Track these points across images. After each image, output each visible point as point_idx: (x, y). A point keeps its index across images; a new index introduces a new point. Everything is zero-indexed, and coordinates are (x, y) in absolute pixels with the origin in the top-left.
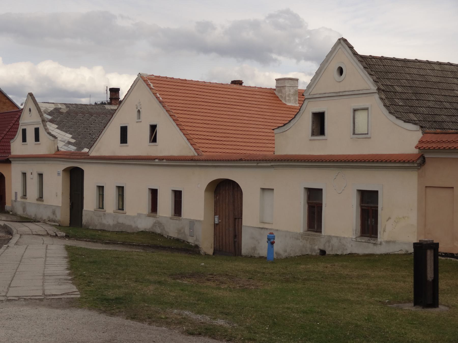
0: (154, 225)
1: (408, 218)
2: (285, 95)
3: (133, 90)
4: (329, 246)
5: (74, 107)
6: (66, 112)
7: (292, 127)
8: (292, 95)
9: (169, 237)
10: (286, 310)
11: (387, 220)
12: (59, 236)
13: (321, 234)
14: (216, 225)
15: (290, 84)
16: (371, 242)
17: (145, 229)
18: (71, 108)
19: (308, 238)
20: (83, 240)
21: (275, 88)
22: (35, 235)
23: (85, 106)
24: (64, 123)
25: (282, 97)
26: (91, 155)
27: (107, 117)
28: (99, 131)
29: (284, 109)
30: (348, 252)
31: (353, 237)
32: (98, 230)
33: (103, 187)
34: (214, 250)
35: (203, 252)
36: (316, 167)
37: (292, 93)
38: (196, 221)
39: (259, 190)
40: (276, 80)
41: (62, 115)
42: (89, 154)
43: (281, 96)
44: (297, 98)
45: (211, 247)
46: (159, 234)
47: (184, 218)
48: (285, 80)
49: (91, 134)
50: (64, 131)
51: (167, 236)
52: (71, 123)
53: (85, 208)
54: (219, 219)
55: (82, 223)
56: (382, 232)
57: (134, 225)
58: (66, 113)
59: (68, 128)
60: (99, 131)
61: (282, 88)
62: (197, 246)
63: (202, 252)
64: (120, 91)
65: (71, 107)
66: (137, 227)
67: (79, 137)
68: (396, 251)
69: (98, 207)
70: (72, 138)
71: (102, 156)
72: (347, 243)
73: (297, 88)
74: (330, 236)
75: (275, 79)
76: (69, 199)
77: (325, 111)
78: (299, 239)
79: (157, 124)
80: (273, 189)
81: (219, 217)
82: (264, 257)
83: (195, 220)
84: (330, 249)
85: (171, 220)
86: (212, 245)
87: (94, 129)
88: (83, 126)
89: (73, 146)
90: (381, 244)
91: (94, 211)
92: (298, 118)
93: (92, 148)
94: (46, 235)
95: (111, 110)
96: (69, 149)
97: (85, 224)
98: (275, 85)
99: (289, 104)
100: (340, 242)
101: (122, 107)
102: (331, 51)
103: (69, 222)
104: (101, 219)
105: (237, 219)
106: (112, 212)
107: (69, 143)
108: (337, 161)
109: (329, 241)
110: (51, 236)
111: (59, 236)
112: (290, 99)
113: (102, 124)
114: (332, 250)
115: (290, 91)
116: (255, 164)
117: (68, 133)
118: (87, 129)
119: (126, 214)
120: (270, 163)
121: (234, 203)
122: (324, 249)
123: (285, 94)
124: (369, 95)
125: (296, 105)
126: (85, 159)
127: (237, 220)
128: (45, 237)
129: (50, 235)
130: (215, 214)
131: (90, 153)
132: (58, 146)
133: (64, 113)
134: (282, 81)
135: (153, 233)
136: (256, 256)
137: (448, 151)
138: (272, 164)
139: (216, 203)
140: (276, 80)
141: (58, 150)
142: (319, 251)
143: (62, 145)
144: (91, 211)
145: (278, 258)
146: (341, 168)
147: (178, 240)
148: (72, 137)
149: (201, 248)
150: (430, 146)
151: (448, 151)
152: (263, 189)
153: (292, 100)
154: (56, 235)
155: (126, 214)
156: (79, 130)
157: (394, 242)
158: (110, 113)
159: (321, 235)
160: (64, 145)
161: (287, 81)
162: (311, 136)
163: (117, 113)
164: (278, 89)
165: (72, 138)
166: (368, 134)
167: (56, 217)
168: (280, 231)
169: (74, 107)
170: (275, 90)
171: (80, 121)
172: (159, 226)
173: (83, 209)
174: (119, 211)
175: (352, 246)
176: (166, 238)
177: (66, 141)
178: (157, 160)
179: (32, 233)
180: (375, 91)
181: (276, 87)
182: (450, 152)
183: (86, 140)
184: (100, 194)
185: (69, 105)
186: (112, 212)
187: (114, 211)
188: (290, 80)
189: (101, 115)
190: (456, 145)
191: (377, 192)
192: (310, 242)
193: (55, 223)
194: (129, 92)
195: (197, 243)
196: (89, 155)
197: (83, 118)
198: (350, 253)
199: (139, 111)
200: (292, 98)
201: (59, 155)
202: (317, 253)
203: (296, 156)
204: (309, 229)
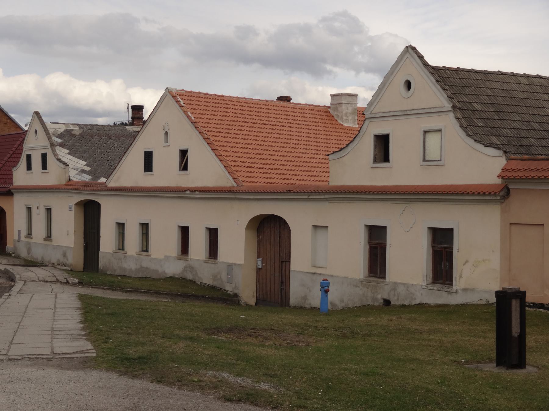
0: (185, 269)
1: (489, 261)
2: (341, 114)
3: (159, 108)
4: (394, 295)
5: (89, 128)
6: (79, 134)
7: (349, 152)
8: (351, 113)
9: (202, 284)
10: (343, 372)
11: (464, 264)
12: (70, 282)
13: (384, 281)
14: (258, 270)
15: (347, 101)
16: (445, 290)
17: (174, 274)
18: (86, 129)
19: (369, 285)
20: (100, 288)
21: (329, 105)
22: (42, 281)
23: (102, 127)
24: (77, 147)
25: (338, 116)
26: (109, 186)
27: (128, 140)
28: (119, 158)
29: (341, 131)
30: (418, 302)
31: (423, 284)
32: (118, 275)
33: (123, 224)
34: (257, 299)
35: (243, 301)
36: (379, 201)
37: (350, 112)
38: (235, 264)
39: (310, 228)
40: (331, 96)
41: (74, 137)
42: (107, 185)
43: (336, 115)
44: (356, 118)
45: (253, 297)
46: (191, 281)
47: (221, 261)
48: (341, 96)
49: (109, 161)
50: (76, 157)
51: (201, 282)
52: (85, 147)
53: (102, 249)
54: (263, 262)
55: (98, 268)
56: (458, 278)
57: (160, 270)
58: (79, 135)
59: (82, 154)
60: (119, 158)
61: (337, 105)
62: (236, 295)
63: (243, 302)
64: (143, 109)
65: (85, 128)
66: (164, 272)
67: (95, 164)
68: (475, 301)
69: (118, 248)
70: (86, 165)
71: (122, 187)
72: (416, 291)
73: (356, 105)
74: (395, 283)
75: (330, 95)
76: (83, 239)
77: (389, 133)
78: (359, 287)
79: (188, 149)
80: (327, 227)
81: (263, 259)
82: (316, 307)
83: (234, 264)
84: (396, 298)
85: (206, 264)
86: (254, 294)
87: (113, 155)
88: (99, 151)
89: (87, 174)
90: (456, 292)
91: (112, 252)
92: (357, 142)
93: (110, 177)
94: (55, 282)
95: (134, 132)
96: (83, 179)
97: (102, 268)
98: (330, 102)
99: (346, 125)
100: (408, 290)
101: (147, 128)
102: (396, 61)
103: (83, 265)
104: (122, 262)
105: (285, 263)
106: (134, 254)
107: (83, 171)
108: (404, 193)
109: (394, 289)
110: (61, 283)
111: (70, 282)
112: (348, 119)
113: (123, 148)
114: (398, 299)
115: (348, 109)
116: (306, 197)
117: (81, 160)
118: (104, 155)
119: (151, 257)
120: (324, 195)
121: (280, 243)
122: (388, 299)
123: (342, 112)
124: (442, 114)
125: (355, 126)
126: (101, 190)
127: (284, 264)
128: (54, 283)
129: (60, 281)
130: (258, 257)
131: (108, 183)
132: (70, 175)
133: (77, 135)
134: (338, 97)
135: (183, 279)
136: (307, 306)
137: (537, 181)
138: (326, 196)
139: (259, 243)
140: (331, 96)
141: (70, 180)
142: (382, 301)
143: (75, 174)
144: (109, 253)
145: (333, 309)
146: (408, 201)
147: (213, 288)
148: (86, 164)
149: (241, 297)
150: (515, 174)
151: (537, 181)
152: (315, 227)
153: (351, 120)
154: (68, 282)
155: (151, 257)
156: (95, 155)
157: (472, 290)
158: (131, 135)
159: (385, 282)
160: (77, 174)
161: (344, 97)
162: (373, 163)
163: (140, 135)
164: (333, 106)
165: (86, 165)
166: (441, 160)
167: (67, 259)
168: (335, 276)
169: (89, 128)
170: (329, 107)
171: (96, 145)
172: (190, 271)
173: (100, 250)
174: (143, 252)
175: (422, 294)
176: (199, 285)
177: (79, 168)
178: (188, 192)
179: (39, 279)
180: (450, 109)
181: (331, 104)
182: (539, 182)
183: (103, 167)
184: (120, 232)
185: (82, 126)
186: (134, 254)
187: (136, 252)
188: (348, 96)
189: (121, 138)
190: (546, 174)
191: (452, 230)
192: (371, 290)
193: (66, 267)
194: (154, 110)
195: (236, 291)
196: (106, 186)
197: (99, 141)
198: (419, 304)
199: (166, 133)
200: (350, 118)
201: (70, 185)
202: (380, 303)
203: (355, 187)
204: (371, 275)
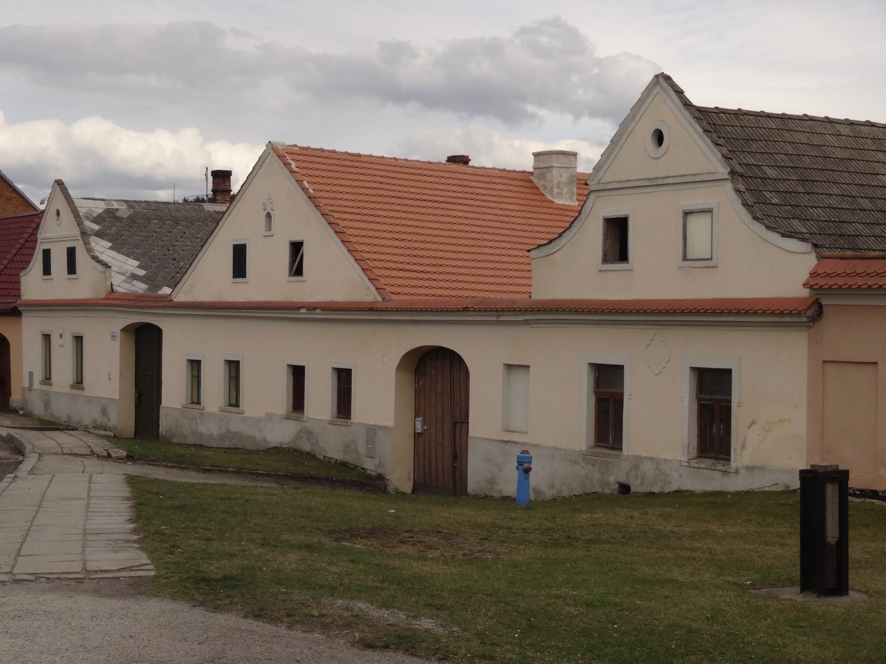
0: (299, 435)
1: (789, 422)
2: (551, 184)
3: (257, 175)
4: (636, 477)
5: (143, 206)
6: (128, 217)
7: (564, 245)
8: (566, 183)
9: (326, 459)
10: (553, 600)
11: (749, 427)
12: (114, 456)
13: (620, 453)
14: (417, 436)
15: (561, 164)
16: (719, 469)
17: (281, 443)
18: (138, 208)
19: (596, 461)
20: (161, 465)
21: (531, 170)
22: (69, 454)
23: (164, 206)
24: (125, 238)
25: (546, 188)
26: (175, 300)
27: (206, 226)
28: (192, 255)
29: (550, 211)
30: (674, 487)
31: (683, 459)
32: (191, 445)
33: (198, 362)
34: (414, 484)
35: (393, 487)
36: (612, 324)
37: (566, 181)
38: (380, 427)
39: (501, 368)
40: (534, 154)
41: (120, 222)
42: (173, 299)
43: (543, 185)
44: (575, 190)
45: (409, 479)
46: (308, 453)
47: (356, 422)
48: (551, 155)
49: (175, 260)
50: (123, 254)
51: (324, 456)
52: (138, 238)
53: (164, 403)
54: (424, 424)
55: (159, 432)
56: (739, 450)
57: (259, 436)
58: (127, 219)
59: (132, 249)
60: (192, 255)
61: (545, 170)
62: (381, 477)
63: (392, 487)
64: (231, 175)
65: (138, 207)
66: (265, 440)
67: (154, 265)
68: (767, 486)
69: (190, 401)
70: (139, 267)
71: (197, 302)
72: (671, 470)
73: (574, 169)
74: (638, 458)
75: (533, 153)
76: (134, 386)
77: (628, 215)
78: (579, 464)
79: (303, 240)
80: (528, 367)
81: (424, 419)
82: (510, 497)
83: (378, 426)
84: (639, 481)
85: (332, 427)
86: (409, 475)
87: (183, 250)
88: (160, 243)
89: (141, 282)
90: (737, 472)
91: (181, 408)
92: (577, 229)
93: (177, 286)
94: (89, 455)
95: (216, 214)
96: (134, 289)
97: (164, 433)
98: (533, 165)
99: (558, 201)
100: (658, 469)
101: (237, 206)
102: (640, 99)
103: (134, 429)
104: (196, 424)
105: (459, 424)
106: (217, 411)
107: (134, 277)
108: (652, 312)
109: (636, 467)
110: (98, 456)
111: (114, 456)
112: (561, 192)
113: (198, 240)
114: (642, 483)
115: (561, 176)
116: (494, 318)
117: (131, 258)
118: (168, 250)
119: (244, 415)
120: (523, 315)
121: (452, 392)
122: (626, 482)
123: (552, 182)
124: (713, 184)
125: (573, 204)
126: (163, 307)
127: (458, 426)
128: (87, 458)
129: (97, 455)
130: (417, 415)
131: (175, 296)
132: (113, 283)
133: (124, 219)
134: (546, 157)
135: (296, 450)
136: (496, 495)
137: (866, 293)
138: (527, 317)
139: (418, 393)
140: (534, 154)
141: (112, 290)
142: (616, 486)
143: (120, 281)
144: (177, 408)
145: (538, 499)
146: (659, 325)
147: (344, 465)
148: (139, 265)
149: (389, 480)
150: (831, 282)
151: (866, 293)
152: (509, 367)
153: (566, 194)
154: (109, 456)
155: (244, 415)
156: (153, 251)
157: (762, 469)
158: (212, 218)
159: (621, 456)
160: (125, 281)
161: (554, 157)
162: (602, 264)
163: (227, 219)
164: (537, 171)
165: (139, 267)
166: (711, 259)
167: (109, 419)
168: (541, 447)
169: (144, 207)
170: (532, 173)
171: (155, 235)
172: (307, 438)
173: (161, 404)
174: (230, 408)
175: (680, 476)
176: (320, 460)
177: (127, 272)
178: (303, 311)
179: (62, 451)
180: (726, 176)
181: (535, 168)
182: (871, 294)
183: (166, 270)
184: (193, 375)
185: (133, 204)
186: (217, 411)
187: (220, 408)
188: (561, 156)
189: (195, 223)
190: (881, 281)
191: (729, 371)
192: (599, 468)
193: (106, 431)
194: (249, 178)
195: (380, 471)
196: (172, 301)
197: (160, 228)
198: (676, 491)
199: (269, 216)
200: (565, 190)
201: (114, 299)
202: (614, 490)
203: (572, 301)
204: (599, 444)
